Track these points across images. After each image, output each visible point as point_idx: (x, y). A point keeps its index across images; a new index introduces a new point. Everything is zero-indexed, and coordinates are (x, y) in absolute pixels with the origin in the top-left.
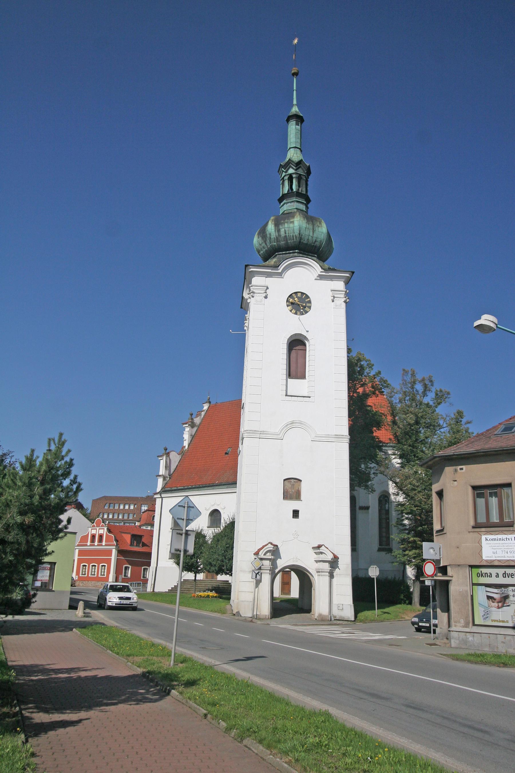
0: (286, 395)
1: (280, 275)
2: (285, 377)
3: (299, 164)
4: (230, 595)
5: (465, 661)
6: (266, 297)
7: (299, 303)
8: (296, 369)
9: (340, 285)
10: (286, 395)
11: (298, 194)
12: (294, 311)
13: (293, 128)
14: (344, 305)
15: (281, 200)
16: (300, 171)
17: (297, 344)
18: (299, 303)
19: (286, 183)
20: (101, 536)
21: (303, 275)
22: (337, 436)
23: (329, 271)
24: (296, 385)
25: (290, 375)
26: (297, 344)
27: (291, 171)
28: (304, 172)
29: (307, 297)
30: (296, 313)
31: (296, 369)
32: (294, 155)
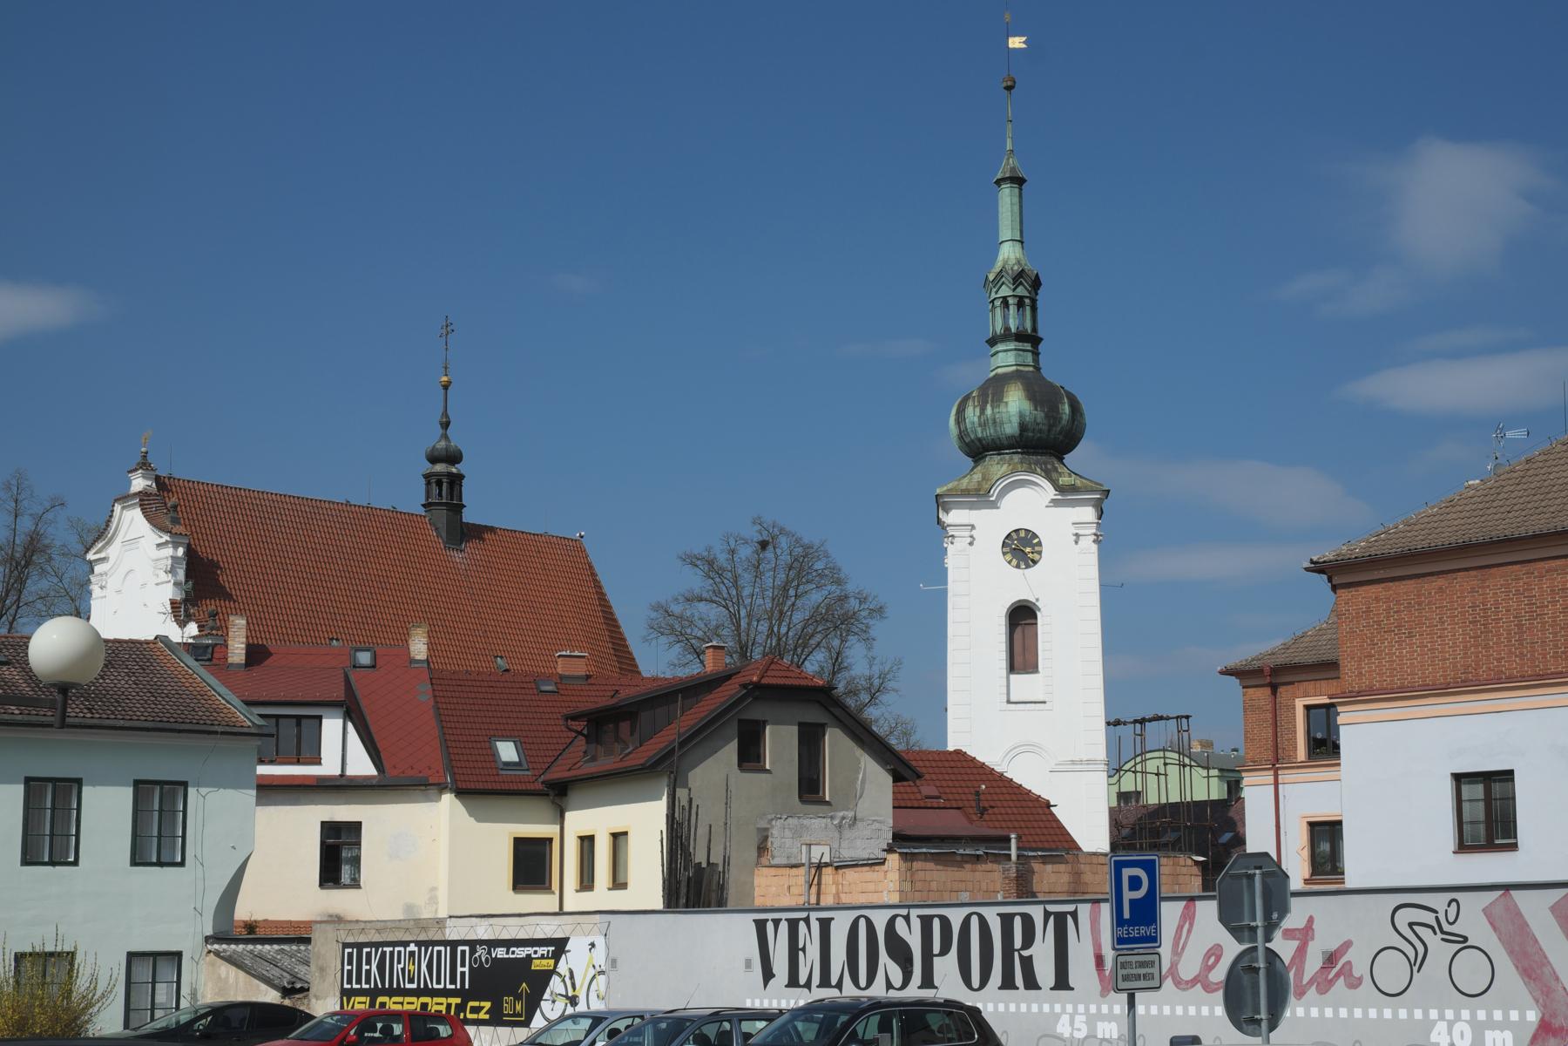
0: (1009, 702)
1: (994, 505)
2: (1004, 672)
3: (1019, 278)
4: (946, 583)
5: (682, 744)
6: (971, 544)
7: (1022, 548)
8: (1021, 658)
9: (1088, 514)
10: (1009, 702)
11: (1020, 337)
12: (1015, 562)
13: (1007, 195)
14: (1094, 547)
15: (992, 342)
16: (1021, 291)
17: (1022, 616)
18: (1022, 548)
19: (998, 311)
20: (587, 883)
21: (1029, 502)
22: (1089, 762)
23: (1067, 493)
24: (1023, 684)
25: (1012, 668)
26: (1022, 616)
27: (1005, 291)
28: (1029, 283)
29: (1035, 536)
30: (1018, 566)
31: (1021, 658)
32: (1009, 253)
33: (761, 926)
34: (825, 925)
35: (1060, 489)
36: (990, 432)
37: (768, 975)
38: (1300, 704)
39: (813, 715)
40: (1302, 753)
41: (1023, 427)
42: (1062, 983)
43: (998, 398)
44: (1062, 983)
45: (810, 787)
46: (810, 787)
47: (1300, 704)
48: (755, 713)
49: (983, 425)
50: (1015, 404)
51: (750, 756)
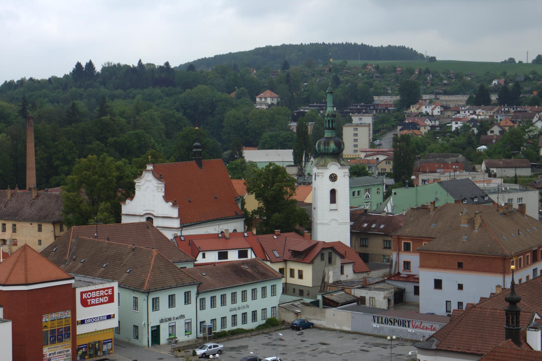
7: (333, 178)
8: (333, 200)
17: (333, 192)
24: (333, 206)
26: (333, 192)
31: (333, 200)
33: (374, 317)
34: (382, 318)
35: (341, 165)
36: (326, 151)
37: (375, 322)
38: (403, 242)
39: (330, 251)
40: (403, 250)
41: (334, 151)
42: (409, 327)
43: (328, 144)
44: (409, 327)
45: (330, 261)
46: (330, 261)
47: (403, 242)
48: (322, 252)
49: (325, 150)
50: (332, 146)
51: (322, 259)
